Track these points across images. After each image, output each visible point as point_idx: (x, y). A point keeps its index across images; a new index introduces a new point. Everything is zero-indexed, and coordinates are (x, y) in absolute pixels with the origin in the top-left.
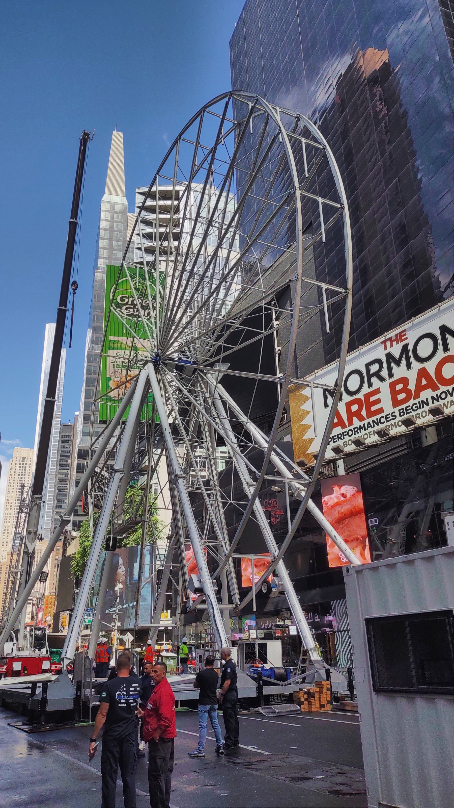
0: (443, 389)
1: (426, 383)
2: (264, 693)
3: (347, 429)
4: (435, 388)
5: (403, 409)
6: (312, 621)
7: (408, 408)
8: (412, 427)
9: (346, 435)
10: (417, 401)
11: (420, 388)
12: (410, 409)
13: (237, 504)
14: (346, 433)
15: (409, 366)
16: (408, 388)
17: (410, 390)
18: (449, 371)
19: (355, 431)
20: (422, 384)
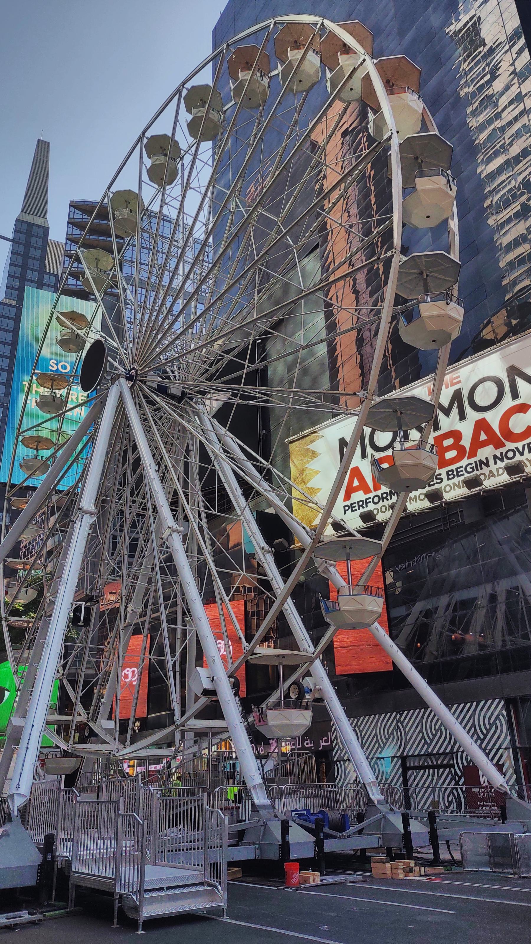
0: (511, 445)
1: (486, 438)
2: (327, 850)
3: (371, 495)
4: (499, 445)
5: (452, 471)
6: (300, 746)
7: (459, 470)
8: (437, 503)
9: (370, 502)
10: (473, 460)
11: (476, 445)
12: (462, 471)
13: (251, 577)
14: (371, 500)
15: (462, 416)
16: (460, 443)
17: (463, 448)
18: (519, 423)
19: (383, 498)
20: (481, 440)
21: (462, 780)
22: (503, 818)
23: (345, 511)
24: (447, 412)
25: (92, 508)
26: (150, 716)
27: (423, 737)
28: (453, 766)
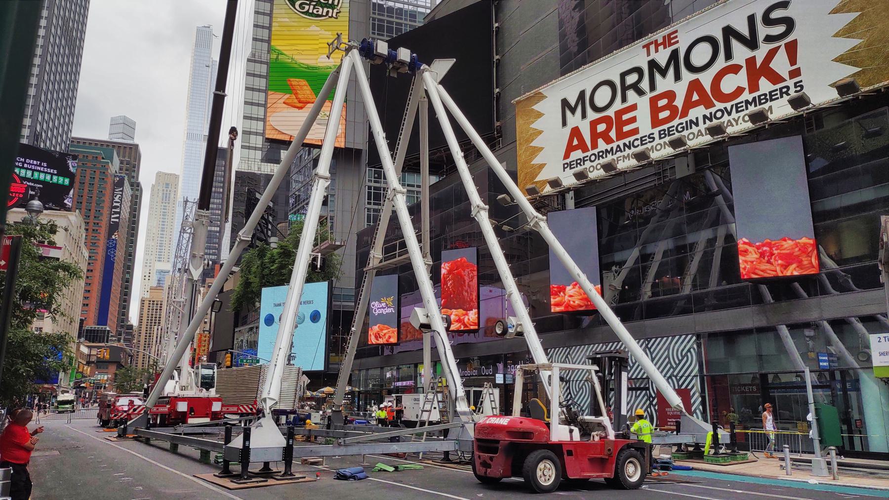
0: (719, 105)
5: (664, 130)
8: (681, 150)
10: (683, 120)
11: (689, 104)
15: (678, 77)
17: (676, 107)
21: (656, 401)
22: (678, 430)
23: (564, 168)
24: (664, 73)
25: (328, 174)
26: (797, 284)
27: (669, 362)
28: (648, 389)
